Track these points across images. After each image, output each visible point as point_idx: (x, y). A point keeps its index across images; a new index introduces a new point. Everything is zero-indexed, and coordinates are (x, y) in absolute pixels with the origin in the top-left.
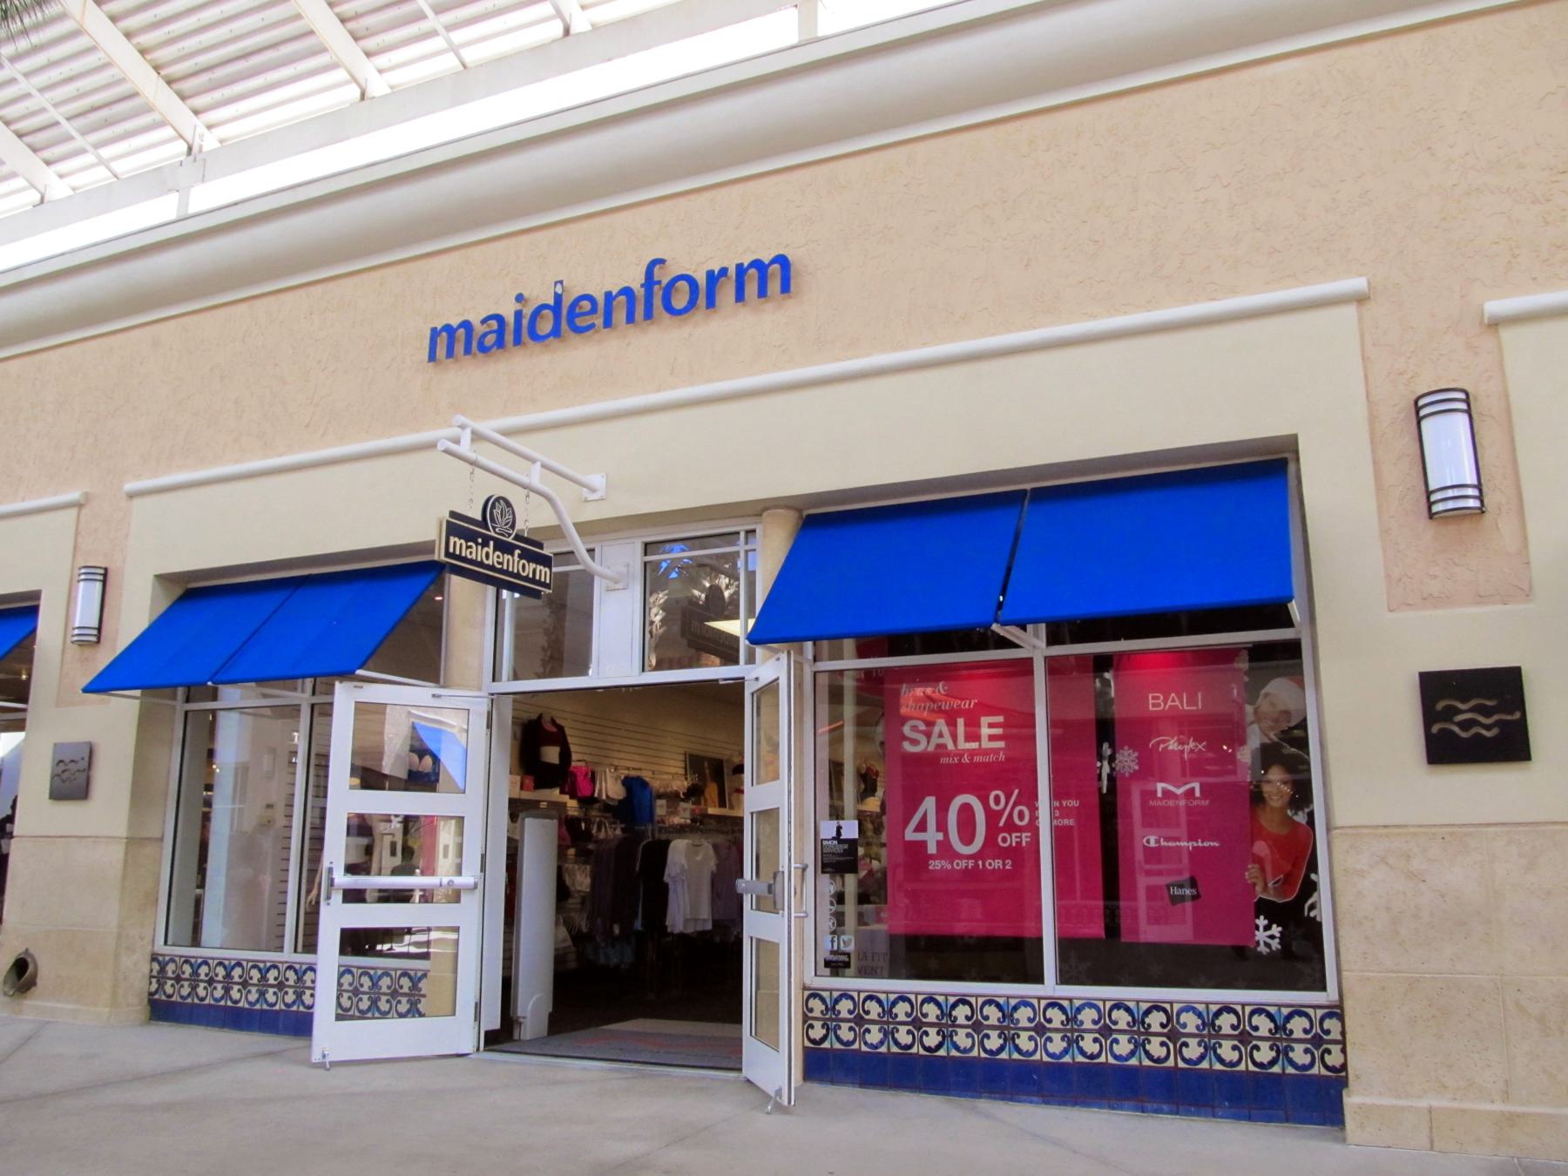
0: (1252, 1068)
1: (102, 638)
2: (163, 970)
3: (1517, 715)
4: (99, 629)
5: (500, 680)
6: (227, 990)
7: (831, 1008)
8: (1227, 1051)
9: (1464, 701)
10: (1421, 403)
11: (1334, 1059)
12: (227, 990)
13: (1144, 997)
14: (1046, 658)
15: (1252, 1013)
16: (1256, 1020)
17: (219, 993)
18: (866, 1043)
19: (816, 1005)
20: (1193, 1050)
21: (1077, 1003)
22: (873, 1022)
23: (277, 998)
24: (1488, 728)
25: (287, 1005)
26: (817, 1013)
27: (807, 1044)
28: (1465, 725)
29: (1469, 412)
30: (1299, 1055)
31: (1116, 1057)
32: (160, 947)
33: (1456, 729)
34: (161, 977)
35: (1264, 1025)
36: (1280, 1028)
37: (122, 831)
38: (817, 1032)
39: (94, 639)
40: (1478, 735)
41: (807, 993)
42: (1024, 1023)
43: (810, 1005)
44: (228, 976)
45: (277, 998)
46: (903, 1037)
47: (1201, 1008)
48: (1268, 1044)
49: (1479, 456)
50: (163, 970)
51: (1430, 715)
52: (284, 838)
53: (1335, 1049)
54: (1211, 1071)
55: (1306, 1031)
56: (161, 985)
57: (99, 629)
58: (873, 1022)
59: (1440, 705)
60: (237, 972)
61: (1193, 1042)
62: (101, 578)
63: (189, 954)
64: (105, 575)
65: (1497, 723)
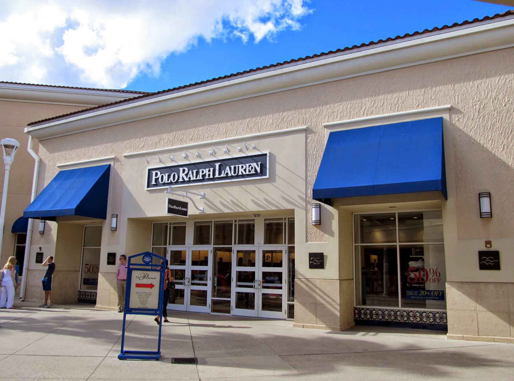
0: (429, 323)
1: (492, 215)
2: (80, 294)
3: (498, 261)
4: (320, 221)
5: (170, 245)
6: (91, 297)
7: (80, 293)
8: (411, 319)
9: (487, 257)
10: (480, 194)
11: (95, 298)
12: (91, 297)
13: (384, 308)
14: (399, 245)
15: (429, 313)
16: (417, 313)
17: (89, 297)
18: (367, 318)
19: (357, 311)
20: (369, 317)
21: (435, 312)
22: (368, 314)
23: (414, 319)
24: (492, 263)
25: (89, 298)
26: (356, 312)
27: (355, 319)
28: (487, 262)
29: (490, 197)
30: (438, 320)
31: (379, 319)
32: (355, 306)
33: (485, 263)
34: (80, 295)
35: (418, 314)
36: (434, 315)
37: (337, 277)
38: (357, 316)
39: (319, 223)
40: (490, 265)
41: (355, 309)
42: (386, 314)
43: (367, 311)
44: (91, 294)
45: (414, 319)
46: (386, 317)
47: (394, 310)
48: (419, 318)
49: (321, 215)
50: (80, 294)
51: (480, 260)
52: (438, 282)
53: (445, 319)
54: (384, 321)
55: (439, 316)
56: (80, 296)
57: (320, 221)
58: (368, 314)
59: (483, 258)
60: (81, 293)
61: (405, 317)
62: (319, 206)
63: (375, 308)
64: (117, 216)
65: (494, 262)
